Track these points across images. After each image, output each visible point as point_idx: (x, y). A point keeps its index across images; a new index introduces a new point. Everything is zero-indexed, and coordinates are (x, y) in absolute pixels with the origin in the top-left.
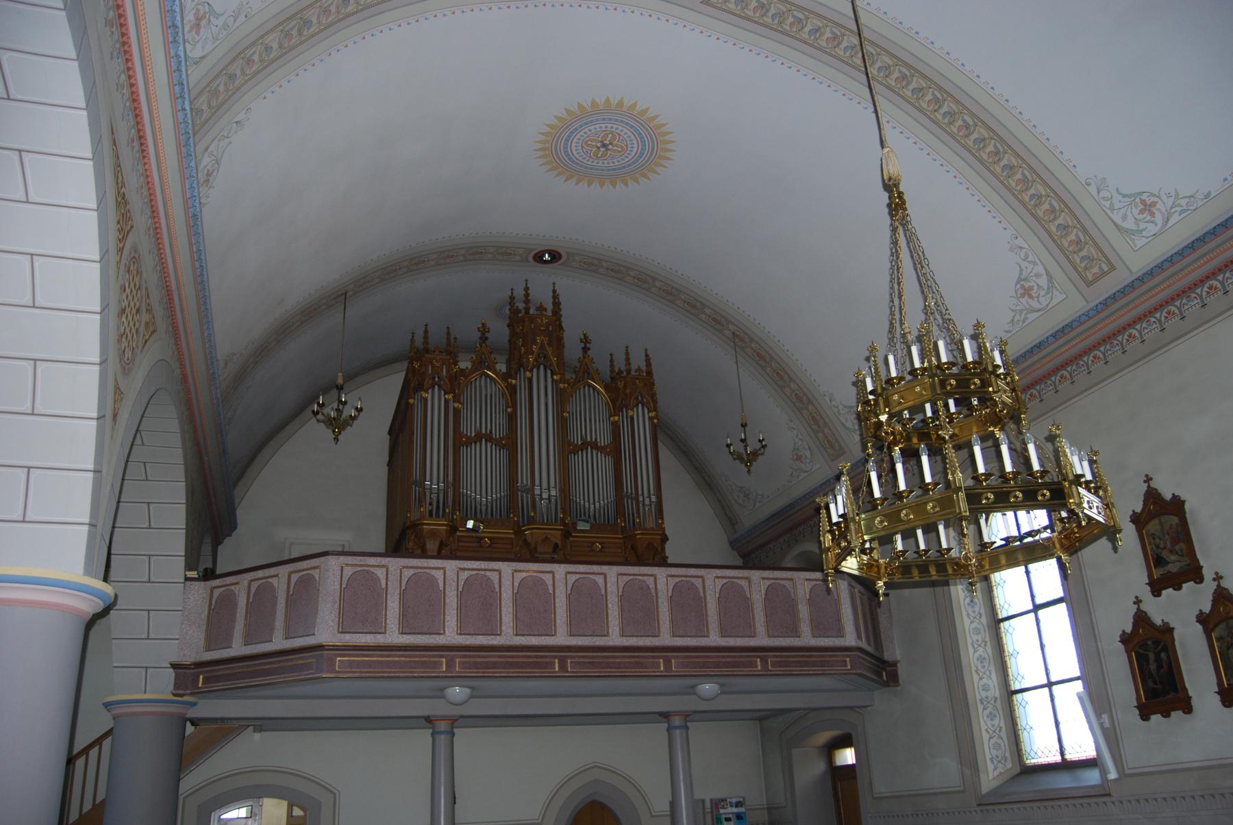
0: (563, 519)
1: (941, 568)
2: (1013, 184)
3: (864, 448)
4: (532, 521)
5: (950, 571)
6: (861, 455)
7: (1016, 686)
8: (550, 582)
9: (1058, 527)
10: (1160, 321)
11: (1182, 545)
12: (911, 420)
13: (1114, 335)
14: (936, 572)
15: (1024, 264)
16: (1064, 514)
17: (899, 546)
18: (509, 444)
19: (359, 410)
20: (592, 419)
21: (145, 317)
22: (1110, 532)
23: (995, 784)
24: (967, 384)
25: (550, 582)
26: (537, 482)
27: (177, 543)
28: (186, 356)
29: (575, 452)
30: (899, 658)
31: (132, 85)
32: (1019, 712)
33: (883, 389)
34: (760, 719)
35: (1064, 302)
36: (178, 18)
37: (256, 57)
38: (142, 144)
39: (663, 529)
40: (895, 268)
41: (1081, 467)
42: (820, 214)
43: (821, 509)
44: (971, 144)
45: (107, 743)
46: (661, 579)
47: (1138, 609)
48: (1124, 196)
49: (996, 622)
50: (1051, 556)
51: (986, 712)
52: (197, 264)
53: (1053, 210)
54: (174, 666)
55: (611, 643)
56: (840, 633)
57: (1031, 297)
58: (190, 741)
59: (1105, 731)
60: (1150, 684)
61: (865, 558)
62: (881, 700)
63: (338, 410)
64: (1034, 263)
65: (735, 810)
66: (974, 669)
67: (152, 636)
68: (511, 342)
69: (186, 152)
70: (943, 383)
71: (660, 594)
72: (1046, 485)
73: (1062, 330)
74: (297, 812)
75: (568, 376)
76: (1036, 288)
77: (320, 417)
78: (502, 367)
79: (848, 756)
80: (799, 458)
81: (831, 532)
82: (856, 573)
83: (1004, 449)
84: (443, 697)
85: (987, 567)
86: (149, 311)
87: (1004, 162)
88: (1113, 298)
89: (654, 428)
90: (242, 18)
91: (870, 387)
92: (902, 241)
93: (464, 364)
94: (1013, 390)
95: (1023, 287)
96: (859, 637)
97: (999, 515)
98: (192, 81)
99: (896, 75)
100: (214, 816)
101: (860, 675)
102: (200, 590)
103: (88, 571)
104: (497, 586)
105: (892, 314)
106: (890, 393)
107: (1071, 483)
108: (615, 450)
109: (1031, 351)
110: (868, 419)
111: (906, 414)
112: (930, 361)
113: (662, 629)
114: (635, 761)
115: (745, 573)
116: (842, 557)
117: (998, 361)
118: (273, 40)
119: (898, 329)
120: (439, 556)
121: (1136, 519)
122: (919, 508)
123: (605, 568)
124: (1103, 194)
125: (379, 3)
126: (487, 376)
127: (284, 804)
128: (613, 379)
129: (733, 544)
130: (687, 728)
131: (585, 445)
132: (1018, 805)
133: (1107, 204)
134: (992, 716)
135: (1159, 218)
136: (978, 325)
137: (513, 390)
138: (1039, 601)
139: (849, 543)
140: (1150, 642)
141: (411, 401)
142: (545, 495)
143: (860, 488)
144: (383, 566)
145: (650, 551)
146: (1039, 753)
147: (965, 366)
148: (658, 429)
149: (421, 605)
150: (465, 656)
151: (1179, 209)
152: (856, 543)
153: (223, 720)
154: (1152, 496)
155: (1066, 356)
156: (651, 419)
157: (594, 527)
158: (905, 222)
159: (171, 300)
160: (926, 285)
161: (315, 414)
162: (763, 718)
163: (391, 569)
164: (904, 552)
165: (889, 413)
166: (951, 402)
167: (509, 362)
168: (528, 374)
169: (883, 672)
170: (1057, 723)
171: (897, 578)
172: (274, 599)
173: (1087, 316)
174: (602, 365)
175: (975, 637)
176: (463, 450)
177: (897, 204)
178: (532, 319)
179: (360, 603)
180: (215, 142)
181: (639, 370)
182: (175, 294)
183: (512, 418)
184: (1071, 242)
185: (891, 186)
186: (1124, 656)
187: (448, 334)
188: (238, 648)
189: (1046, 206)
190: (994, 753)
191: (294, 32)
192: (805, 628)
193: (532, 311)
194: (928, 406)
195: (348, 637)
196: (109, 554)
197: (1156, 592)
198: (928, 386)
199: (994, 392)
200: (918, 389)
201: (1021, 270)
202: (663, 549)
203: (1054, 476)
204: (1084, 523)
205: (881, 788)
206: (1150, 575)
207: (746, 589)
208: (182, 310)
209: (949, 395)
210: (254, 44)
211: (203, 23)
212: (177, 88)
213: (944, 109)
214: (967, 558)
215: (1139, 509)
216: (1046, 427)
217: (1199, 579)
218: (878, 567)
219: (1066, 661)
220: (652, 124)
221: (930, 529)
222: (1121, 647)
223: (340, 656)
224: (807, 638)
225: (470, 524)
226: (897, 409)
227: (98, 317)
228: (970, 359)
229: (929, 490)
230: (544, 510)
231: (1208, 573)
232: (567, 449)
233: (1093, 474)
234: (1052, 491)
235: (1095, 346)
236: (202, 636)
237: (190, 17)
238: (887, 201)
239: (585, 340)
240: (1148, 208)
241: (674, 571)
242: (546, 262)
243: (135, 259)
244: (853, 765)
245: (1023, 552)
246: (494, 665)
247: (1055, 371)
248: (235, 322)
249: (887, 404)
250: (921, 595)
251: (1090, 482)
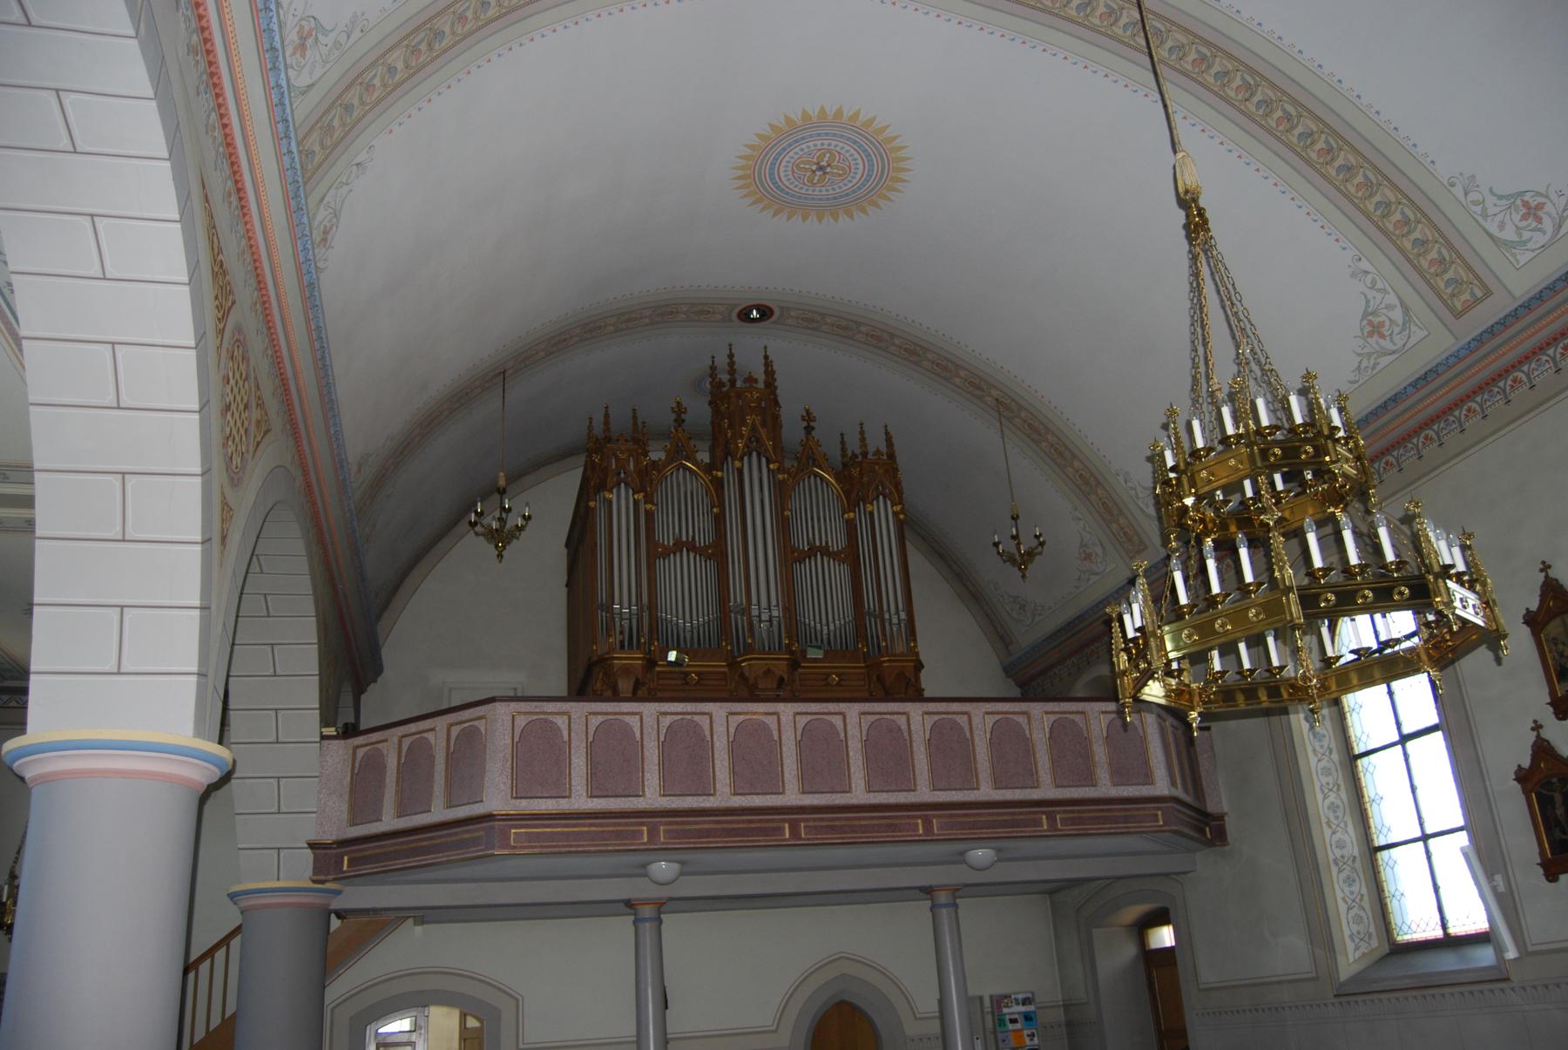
0: (789, 646)
1: (1274, 692)
2: (1353, 190)
3: (1166, 541)
4: (749, 649)
5: (1285, 696)
6: (1163, 553)
7: (1380, 841)
8: (774, 727)
9: (1425, 633)
10: (1554, 359)
12: (1226, 502)
13: (1493, 380)
14: (1270, 697)
16: (1431, 618)
17: (1217, 665)
18: (717, 553)
19: (527, 519)
20: (821, 520)
21: (256, 414)
22: (1491, 638)
23: (1356, 968)
24: (1296, 452)
25: (774, 727)
26: (754, 600)
27: (309, 694)
28: (309, 457)
29: (801, 561)
30: (1226, 808)
31: (225, 126)
32: (1386, 874)
33: (1187, 464)
34: (1051, 893)
35: (1428, 340)
36: (277, 38)
37: (377, 82)
38: (241, 199)
39: (917, 654)
40: (1198, 307)
41: (1448, 554)
42: (1098, 243)
43: (1109, 623)
44: (1295, 140)
45: (236, 943)
46: (916, 718)
47: (1538, 736)
48: (1500, 197)
49: (1351, 758)
50: (1417, 671)
51: (1343, 875)
52: (317, 345)
53: (1407, 222)
54: (312, 846)
55: (854, 801)
56: (1148, 779)
57: (1382, 336)
58: (337, 938)
59: (1499, 897)
60: (1557, 833)
61: (1173, 682)
62: (1204, 862)
63: (500, 519)
64: (1384, 291)
65: (1022, 1009)
66: (1324, 820)
67: (283, 809)
68: (715, 424)
69: (295, 207)
70: (1264, 453)
71: (915, 736)
72: (1404, 581)
73: (1425, 377)
74: (472, 1023)
75: (788, 464)
76: (1387, 323)
77: (478, 528)
78: (704, 457)
79: (1165, 937)
80: (1088, 557)
81: (1127, 650)
82: (1163, 702)
83: (1348, 536)
84: (646, 875)
85: (1334, 688)
86: (260, 405)
87: (1339, 162)
88: (1491, 332)
89: (901, 527)
90: (357, 34)
91: (1170, 463)
92: (1205, 271)
93: (657, 455)
94: (1358, 458)
95: (1370, 323)
96: (1173, 784)
97: (1347, 619)
98: (300, 115)
99: (1193, 56)
100: (370, 1031)
101: (1175, 832)
102: (339, 750)
103: (199, 732)
104: (707, 733)
105: (1195, 366)
106: (1196, 468)
107: (1437, 576)
108: (851, 556)
109: (1384, 407)
110: (1170, 504)
111: (1219, 495)
112: (1246, 426)
113: (919, 781)
114: (892, 953)
115: (1023, 706)
116: (1141, 684)
117: (1337, 422)
118: (397, 59)
119: (1204, 386)
120: (635, 697)
121: (1531, 620)
122: (1238, 616)
123: (843, 707)
124: (1471, 197)
125: (527, 4)
126: (686, 468)
127: (455, 1015)
128: (845, 465)
129: (1008, 670)
130: (956, 906)
131: (813, 551)
132: (1414, 993)
133: (1478, 209)
134: (1349, 881)
135: (1548, 225)
136: (1308, 376)
137: (719, 484)
138: (1406, 730)
139: (1149, 664)
141: (592, 504)
142: (765, 617)
143: (1162, 595)
144: (564, 713)
145: (903, 683)
146: (1414, 927)
147: (1293, 429)
148: (903, 527)
149: (614, 761)
150: (671, 823)
152: (1158, 664)
153: (375, 911)
155: (1430, 411)
156: (895, 514)
157: (830, 654)
158: (1208, 247)
159: (287, 390)
160: (1239, 328)
161: (473, 525)
162: (1054, 890)
163: (912, 714)
164: (1223, 673)
165: (1195, 494)
166: (1278, 478)
167: (712, 451)
168: (737, 464)
169: (1207, 828)
170: (1437, 889)
171: (1214, 708)
172: (431, 759)
173: (1458, 357)
174: (831, 449)
175: (1324, 780)
176: (659, 563)
177: (1196, 225)
178: (739, 395)
179: (538, 760)
180: (332, 192)
181: (878, 452)
182: (292, 383)
183: (719, 521)
184: (1432, 262)
185: (1187, 201)
186: (1521, 799)
187: (635, 417)
188: (389, 821)
189: (1397, 216)
190: (1355, 928)
191: (423, 47)
192: (1103, 774)
193: (739, 384)
194: (1247, 484)
195: (524, 802)
196: (225, 709)
198: (1245, 457)
199: (1332, 462)
200: (1232, 462)
201: (1368, 301)
202: (918, 679)
203: (1412, 568)
204: (1455, 628)
205: (1208, 976)
206: (1552, 692)
207: (1026, 727)
208: (301, 403)
209: (1274, 468)
210: (373, 65)
211: (309, 42)
212: (280, 126)
213: (1258, 97)
214: (1305, 678)
215: (1534, 605)
216: (1404, 505)
218: (1190, 693)
219: (1445, 806)
220: (880, 138)
221: (1257, 642)
222: (1517, 786)
223: (516, 827)
224: (1105, 788)
225: (672, 656)
226: (1207, 489)
227: (197, 416)
228: (1299, 420)
229: (1250, 592)
230: (764, 635)
232: (791, 557)
233: (1467, 563)
234: (1416, 586)
235: (1469, 397)
236: (345, 807)
237: (292, 36)
238: (1183, 221)
239: (808, 417)
240: (1532, 212)
241: (932, 707)
242: (754, 320)
243: (239, 342)
244: (1171, 949)
245: (1382, 666)
246: (708, 833)
247: (1417, 431)
248: (367, 417)
249: (1193, 484)
250: (1252, 729)
251: (1463, 573)
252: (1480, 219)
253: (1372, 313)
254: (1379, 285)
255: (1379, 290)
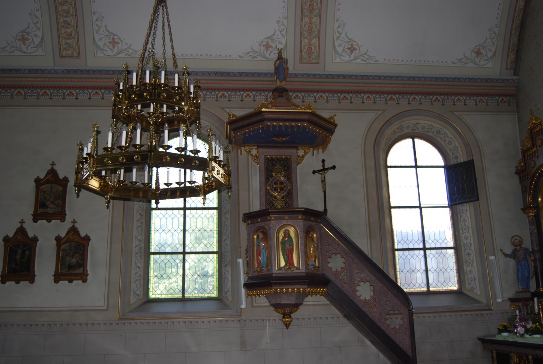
11: (60, 202)
15: (278, 33)
48: (107, 31)
76: (31, 40)
95: (23, 36)
124: (98, 23)
132: (461, 313)
133: (97, 28)
135: (115, 50)
140: (21, 244)
151: (127, 52)
154: (52, 173)
173: (49, 71)
189: (66, 8)
197: (35, 220)
217: (63, 220)
219: (533, 265)
231: (69, 218)
240: (352, 49)
251: (221, 161)
252: (95, 32)
253: (26, 33)
254: (38, 25)
255: (36, 27)
